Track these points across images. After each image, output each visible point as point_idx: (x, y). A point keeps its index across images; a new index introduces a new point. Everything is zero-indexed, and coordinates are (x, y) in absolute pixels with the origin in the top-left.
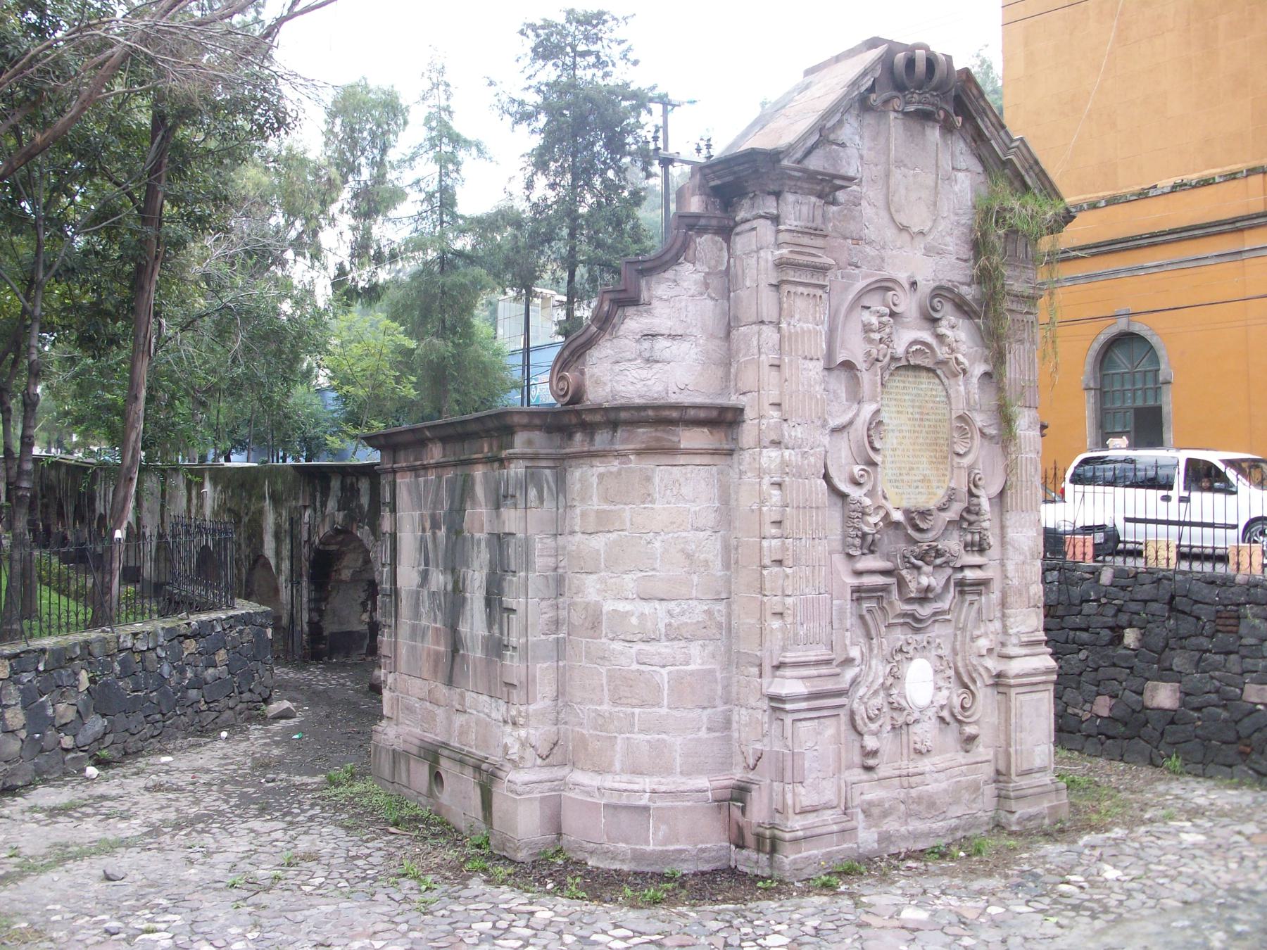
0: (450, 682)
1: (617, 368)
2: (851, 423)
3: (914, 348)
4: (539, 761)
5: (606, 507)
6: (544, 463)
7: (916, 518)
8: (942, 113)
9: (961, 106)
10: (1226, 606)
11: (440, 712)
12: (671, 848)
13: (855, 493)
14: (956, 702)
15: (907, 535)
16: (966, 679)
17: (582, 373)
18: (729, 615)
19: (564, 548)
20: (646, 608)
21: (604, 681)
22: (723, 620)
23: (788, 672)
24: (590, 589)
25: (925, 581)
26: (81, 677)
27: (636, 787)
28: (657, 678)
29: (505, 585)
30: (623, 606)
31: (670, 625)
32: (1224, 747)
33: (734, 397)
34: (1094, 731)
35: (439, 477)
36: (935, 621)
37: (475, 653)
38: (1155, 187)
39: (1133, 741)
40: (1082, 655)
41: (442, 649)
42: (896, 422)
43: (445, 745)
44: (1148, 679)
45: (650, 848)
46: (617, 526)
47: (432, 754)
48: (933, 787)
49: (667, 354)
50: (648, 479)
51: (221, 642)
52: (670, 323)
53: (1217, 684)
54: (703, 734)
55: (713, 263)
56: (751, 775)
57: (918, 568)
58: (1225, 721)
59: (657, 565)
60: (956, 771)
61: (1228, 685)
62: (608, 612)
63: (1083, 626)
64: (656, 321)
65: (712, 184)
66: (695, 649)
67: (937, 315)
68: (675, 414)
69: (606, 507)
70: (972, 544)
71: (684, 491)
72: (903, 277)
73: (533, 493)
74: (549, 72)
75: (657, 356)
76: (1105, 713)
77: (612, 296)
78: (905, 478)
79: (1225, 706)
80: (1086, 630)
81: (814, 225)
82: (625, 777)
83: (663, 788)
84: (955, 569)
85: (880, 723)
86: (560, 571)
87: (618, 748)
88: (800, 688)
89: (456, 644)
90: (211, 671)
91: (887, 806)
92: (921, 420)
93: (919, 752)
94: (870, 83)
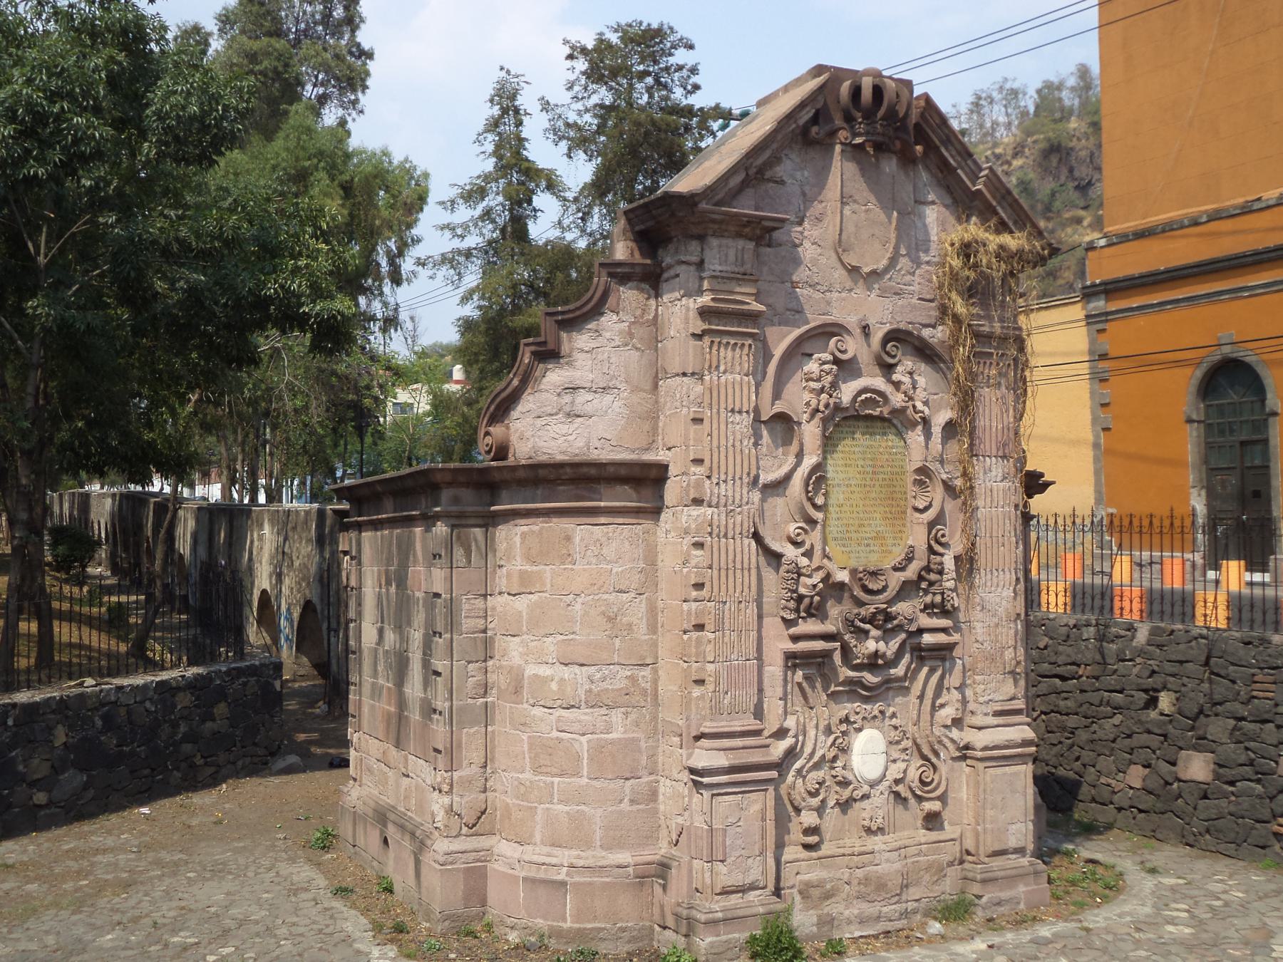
0: (398, 745)
1: (539, 422)
2: (788, 477)
3: (863, 397)
4: (465, 829)
5: (528, 568)
6: (472, 521)
7: (866, 578)
8: (898, 143)
9: (921, 134)
10: (1262, 669)
11: (390, 773)
12: (589, 926)
13: (790, 552)
14: (913, 774)
15: (853, 597)
16: (926, 751)
17: (508, 428)
18: (655, 682)
19: (494, 609)
20: (566, 672)
21: (526, 746)
22: (648, 686)
23: (704, 742)
24: (512, 651)
25: (871, 645)
26: (56, 732)
27: (554, 861)
28: (577, 746)
29: (433, 646)
30: (545, 671)
31: (590, 691)
32: (1258, 825)
33: (661, 453)
34: (1126, 804)
35: (391, 534)
36: (888, 689)
37: (415, 716)
38: (1259, 199)
39: (1166, 816)
40: (1118, 719)
41: (393, 709)
42: (842, 476)
43: (393, 809)
44: (1181, 749)
45: (568, 924)
46: (538, 588)
47: (382, 816)
48: (883, 868)
49: (588, 409)
50: (568, 538)
51: (221, 694)
52: (591, 376)
53: (1253, 756)
54: (625, 806)
55: (638, 312)
56: (674, 851)
57: (866, 632)
58: (1260, 797)
59: (577, 629)
60: (913, 850)
61: (1263, 757)
62: (529, 677)
63: (1118, 688)
64: (578, 374)
65: (637, 228)
66: (617, 716)
67: (892, 361)
68: (593, 471)
69: (528, 568)
70: (933, 605)
71: (604, 551)
72: (851, 321)
73: (459, 553)
74: (603, 95)
75: (578, 409)
76: (1137, 784)
77: (533, 348)
78: (854, 535)
79: (1258, 781)
80: (1120, 692)
81: (742, 270)
82: (547, 849)
83: (581, 863)
84: (910, 634)
85: (821, 797)
86: (490, 633)
87: (538, 818)
88: (722, 761)
89: (402, 704)
90: (209, 725)
91: (828, 887)
92: (874, 473)
93: (869, 831)
94: (811, 114)
